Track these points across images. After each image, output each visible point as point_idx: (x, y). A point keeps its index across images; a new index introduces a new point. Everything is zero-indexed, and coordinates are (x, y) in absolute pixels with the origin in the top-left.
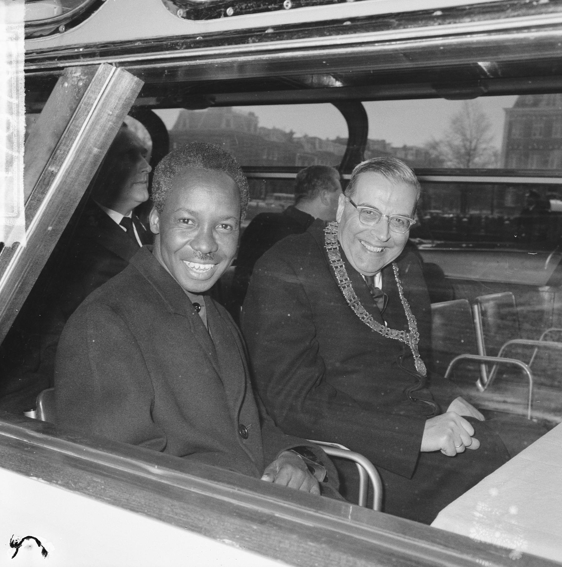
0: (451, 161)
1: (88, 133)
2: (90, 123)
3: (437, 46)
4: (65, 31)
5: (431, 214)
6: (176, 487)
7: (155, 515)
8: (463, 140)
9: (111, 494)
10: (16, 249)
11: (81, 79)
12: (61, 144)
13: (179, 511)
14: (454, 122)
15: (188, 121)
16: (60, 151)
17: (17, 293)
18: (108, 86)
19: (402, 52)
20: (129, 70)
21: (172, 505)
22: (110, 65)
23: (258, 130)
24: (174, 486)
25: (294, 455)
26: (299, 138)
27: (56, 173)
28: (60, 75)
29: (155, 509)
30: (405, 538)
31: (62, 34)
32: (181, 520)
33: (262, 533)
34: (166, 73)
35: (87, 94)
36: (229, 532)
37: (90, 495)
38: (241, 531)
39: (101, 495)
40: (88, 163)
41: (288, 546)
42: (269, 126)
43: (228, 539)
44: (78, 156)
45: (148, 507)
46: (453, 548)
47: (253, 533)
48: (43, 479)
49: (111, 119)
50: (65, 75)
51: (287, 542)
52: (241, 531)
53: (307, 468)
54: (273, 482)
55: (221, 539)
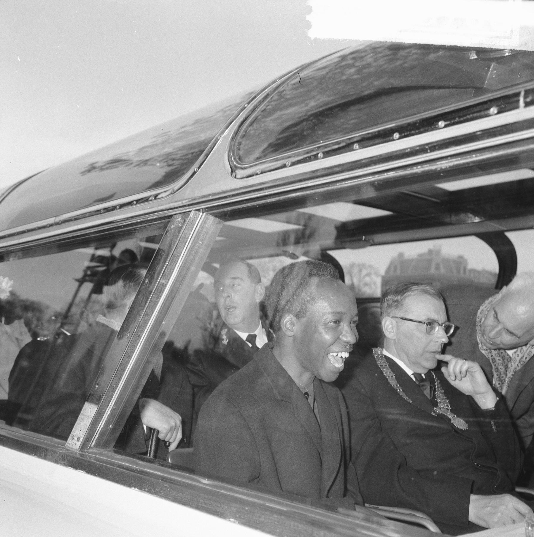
15: (399, 267)
20: (210, 214)
22: (198, 212)
23: (467, 273)
27: (166, 285)
32: (208, 508)
37: (161, 496)
43: (232, 518)
45: (191, 501)
48: (137, 488)
51: (263, 516)
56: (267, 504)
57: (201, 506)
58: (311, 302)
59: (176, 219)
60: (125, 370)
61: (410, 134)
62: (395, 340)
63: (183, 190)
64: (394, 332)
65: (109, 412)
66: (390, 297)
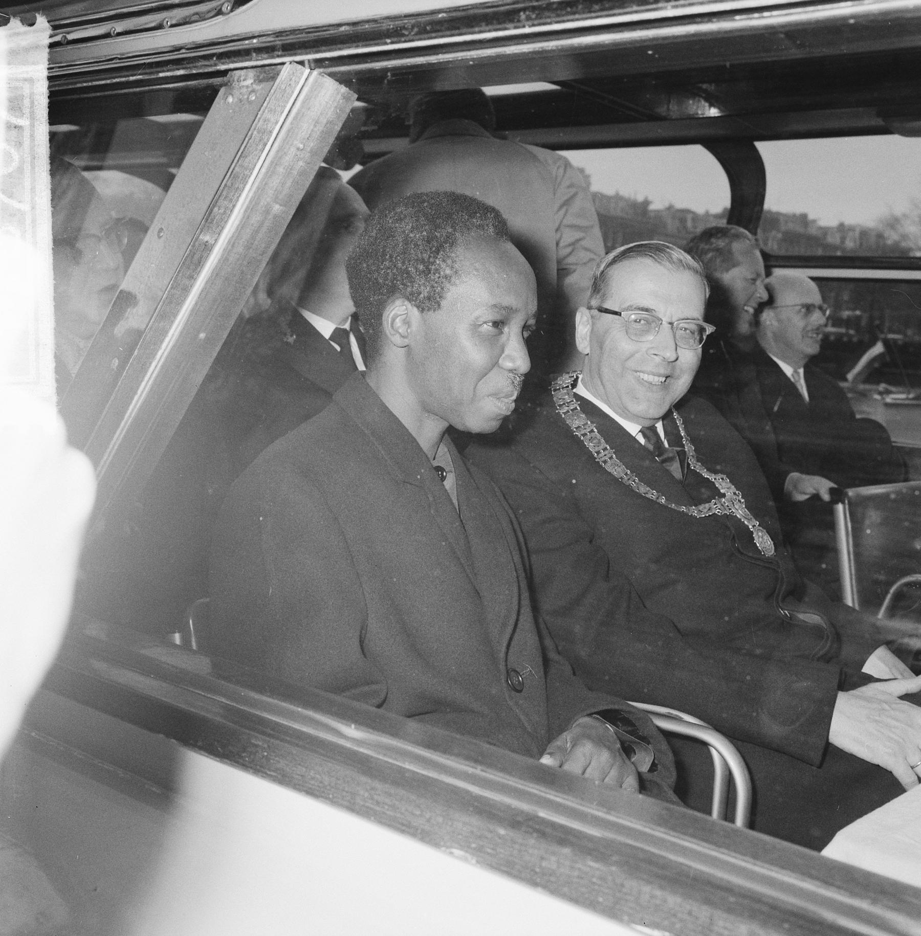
1: (263, 179)
2: (267, 162)
3: (844, 19)
4: (232, 11)
6: (381, 760)
7: (345, 803)
11: (253, 91)
12: (219, 197)
13: (380, 799)
16: (219, 209)
18: (297, 101)
19: (783, 30)
20: (331, 75)
21: (372, 789)
22: (300, 67)
24: (378, 759)
25: (597, 724)
26: (658, 211)
27: (213, 246)
29: (344, 794)
30: (755, 864)
31: (227, 17)
32: (384, 813)
34: (389, 77)
35: (262, 115)
36: (460, 837)
38: (480, 837)
39: (261, 766)
40: (264, 229)
41: (554, 867)
46: (839, 887)
47: (499, 841)
49: (302, 156)
50: (229, 84)
51: (553, 859)
52: (480, 837)
53: (618, 746)
54: (560, 767)
55: (447, 847)
58: (453, 279)
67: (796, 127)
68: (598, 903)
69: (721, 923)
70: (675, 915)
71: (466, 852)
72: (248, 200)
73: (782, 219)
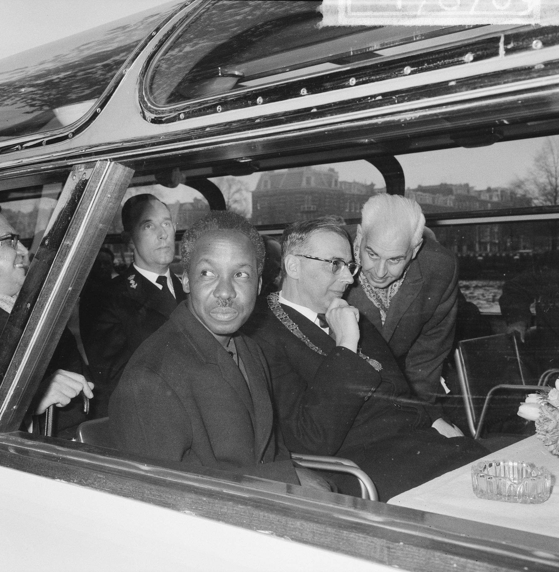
0: (537, 199)
5: (521, 254)
8: (548, 177)
9: (110, 486)
10: (45, 306)
13: (155, 493)
14: (537, 160)
17: (49, 341)
20: (121, 163)
21: (151, 489)
28: (70, 171)
33: (209, 503)
37: (96, 488)
42: (350, 180)
44: (87, 231)
51: (225, 507)
55: (183, 510)
56: (224, 491)
57: (148, 498)
59: (78, 169)
60: (28, 345)
61: (369, 80)
62: (298, 279)
63: (83, 133)
64: (298, 270)
65: (12, 393)
66: (293, 234)
67: (412, 147)
68: (244, 523)
69: (290, 523)
70: (273, 523)
71: (191, 511)
72: (86, 223)
73: (454, 188)
